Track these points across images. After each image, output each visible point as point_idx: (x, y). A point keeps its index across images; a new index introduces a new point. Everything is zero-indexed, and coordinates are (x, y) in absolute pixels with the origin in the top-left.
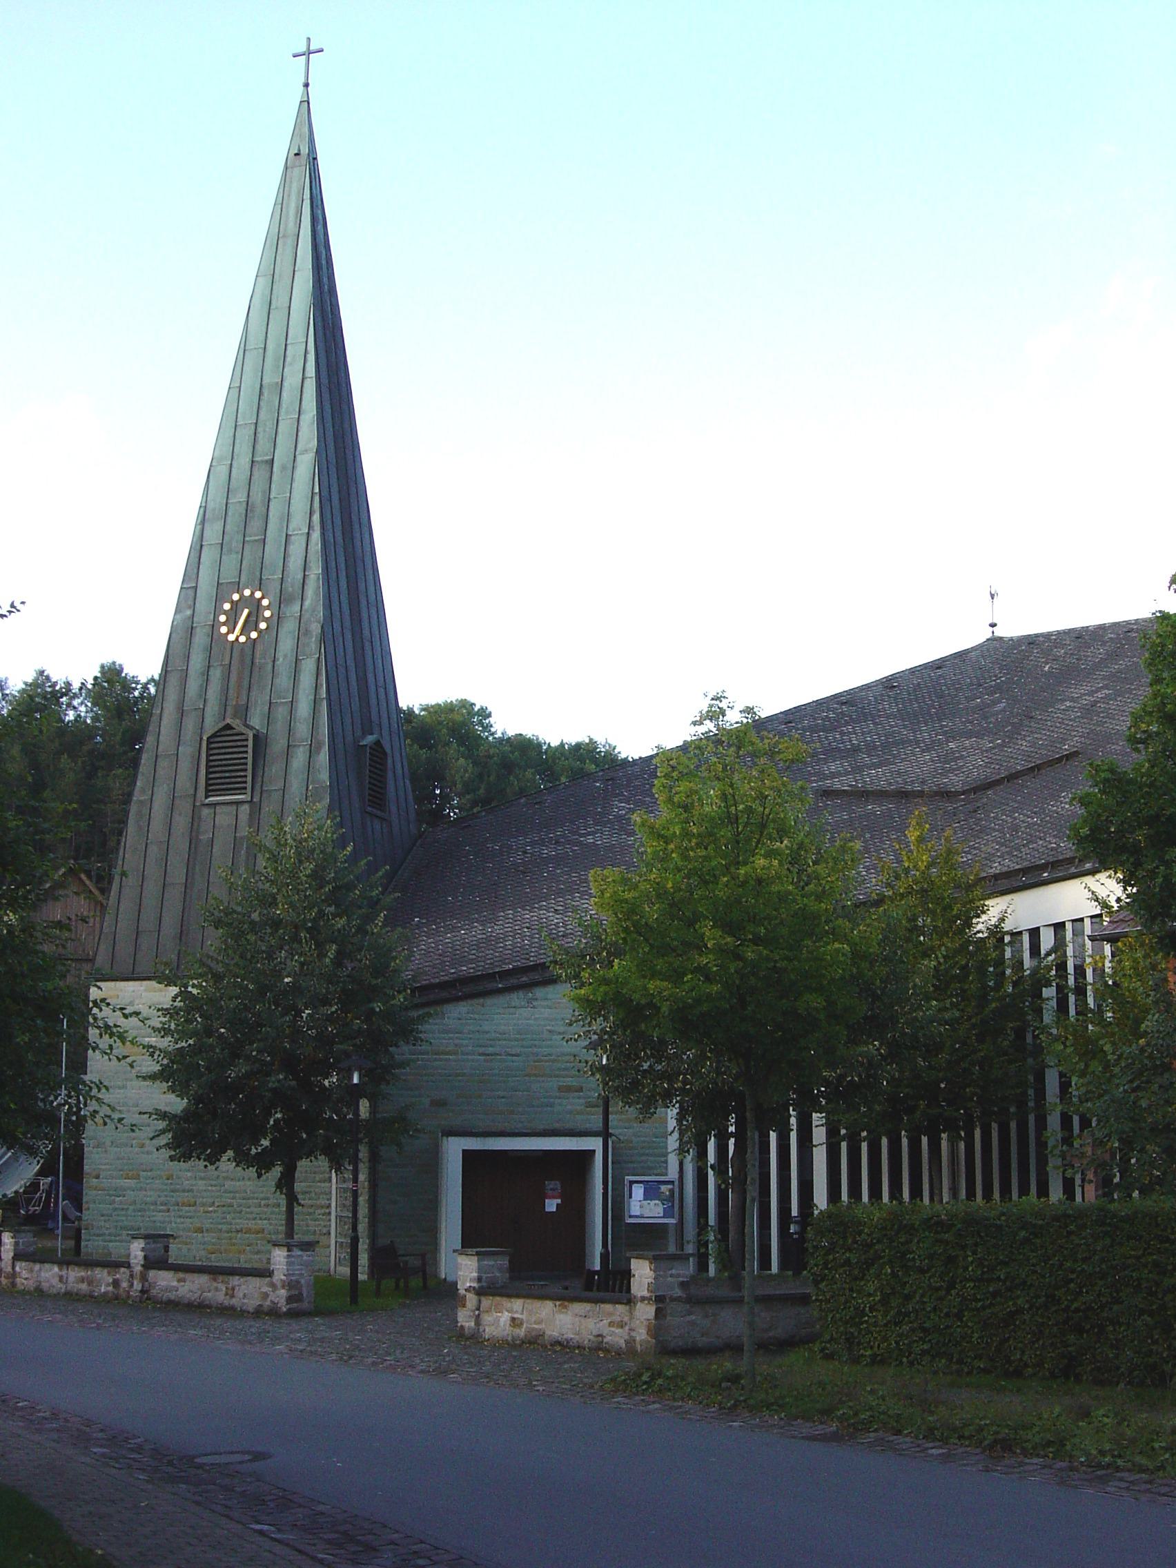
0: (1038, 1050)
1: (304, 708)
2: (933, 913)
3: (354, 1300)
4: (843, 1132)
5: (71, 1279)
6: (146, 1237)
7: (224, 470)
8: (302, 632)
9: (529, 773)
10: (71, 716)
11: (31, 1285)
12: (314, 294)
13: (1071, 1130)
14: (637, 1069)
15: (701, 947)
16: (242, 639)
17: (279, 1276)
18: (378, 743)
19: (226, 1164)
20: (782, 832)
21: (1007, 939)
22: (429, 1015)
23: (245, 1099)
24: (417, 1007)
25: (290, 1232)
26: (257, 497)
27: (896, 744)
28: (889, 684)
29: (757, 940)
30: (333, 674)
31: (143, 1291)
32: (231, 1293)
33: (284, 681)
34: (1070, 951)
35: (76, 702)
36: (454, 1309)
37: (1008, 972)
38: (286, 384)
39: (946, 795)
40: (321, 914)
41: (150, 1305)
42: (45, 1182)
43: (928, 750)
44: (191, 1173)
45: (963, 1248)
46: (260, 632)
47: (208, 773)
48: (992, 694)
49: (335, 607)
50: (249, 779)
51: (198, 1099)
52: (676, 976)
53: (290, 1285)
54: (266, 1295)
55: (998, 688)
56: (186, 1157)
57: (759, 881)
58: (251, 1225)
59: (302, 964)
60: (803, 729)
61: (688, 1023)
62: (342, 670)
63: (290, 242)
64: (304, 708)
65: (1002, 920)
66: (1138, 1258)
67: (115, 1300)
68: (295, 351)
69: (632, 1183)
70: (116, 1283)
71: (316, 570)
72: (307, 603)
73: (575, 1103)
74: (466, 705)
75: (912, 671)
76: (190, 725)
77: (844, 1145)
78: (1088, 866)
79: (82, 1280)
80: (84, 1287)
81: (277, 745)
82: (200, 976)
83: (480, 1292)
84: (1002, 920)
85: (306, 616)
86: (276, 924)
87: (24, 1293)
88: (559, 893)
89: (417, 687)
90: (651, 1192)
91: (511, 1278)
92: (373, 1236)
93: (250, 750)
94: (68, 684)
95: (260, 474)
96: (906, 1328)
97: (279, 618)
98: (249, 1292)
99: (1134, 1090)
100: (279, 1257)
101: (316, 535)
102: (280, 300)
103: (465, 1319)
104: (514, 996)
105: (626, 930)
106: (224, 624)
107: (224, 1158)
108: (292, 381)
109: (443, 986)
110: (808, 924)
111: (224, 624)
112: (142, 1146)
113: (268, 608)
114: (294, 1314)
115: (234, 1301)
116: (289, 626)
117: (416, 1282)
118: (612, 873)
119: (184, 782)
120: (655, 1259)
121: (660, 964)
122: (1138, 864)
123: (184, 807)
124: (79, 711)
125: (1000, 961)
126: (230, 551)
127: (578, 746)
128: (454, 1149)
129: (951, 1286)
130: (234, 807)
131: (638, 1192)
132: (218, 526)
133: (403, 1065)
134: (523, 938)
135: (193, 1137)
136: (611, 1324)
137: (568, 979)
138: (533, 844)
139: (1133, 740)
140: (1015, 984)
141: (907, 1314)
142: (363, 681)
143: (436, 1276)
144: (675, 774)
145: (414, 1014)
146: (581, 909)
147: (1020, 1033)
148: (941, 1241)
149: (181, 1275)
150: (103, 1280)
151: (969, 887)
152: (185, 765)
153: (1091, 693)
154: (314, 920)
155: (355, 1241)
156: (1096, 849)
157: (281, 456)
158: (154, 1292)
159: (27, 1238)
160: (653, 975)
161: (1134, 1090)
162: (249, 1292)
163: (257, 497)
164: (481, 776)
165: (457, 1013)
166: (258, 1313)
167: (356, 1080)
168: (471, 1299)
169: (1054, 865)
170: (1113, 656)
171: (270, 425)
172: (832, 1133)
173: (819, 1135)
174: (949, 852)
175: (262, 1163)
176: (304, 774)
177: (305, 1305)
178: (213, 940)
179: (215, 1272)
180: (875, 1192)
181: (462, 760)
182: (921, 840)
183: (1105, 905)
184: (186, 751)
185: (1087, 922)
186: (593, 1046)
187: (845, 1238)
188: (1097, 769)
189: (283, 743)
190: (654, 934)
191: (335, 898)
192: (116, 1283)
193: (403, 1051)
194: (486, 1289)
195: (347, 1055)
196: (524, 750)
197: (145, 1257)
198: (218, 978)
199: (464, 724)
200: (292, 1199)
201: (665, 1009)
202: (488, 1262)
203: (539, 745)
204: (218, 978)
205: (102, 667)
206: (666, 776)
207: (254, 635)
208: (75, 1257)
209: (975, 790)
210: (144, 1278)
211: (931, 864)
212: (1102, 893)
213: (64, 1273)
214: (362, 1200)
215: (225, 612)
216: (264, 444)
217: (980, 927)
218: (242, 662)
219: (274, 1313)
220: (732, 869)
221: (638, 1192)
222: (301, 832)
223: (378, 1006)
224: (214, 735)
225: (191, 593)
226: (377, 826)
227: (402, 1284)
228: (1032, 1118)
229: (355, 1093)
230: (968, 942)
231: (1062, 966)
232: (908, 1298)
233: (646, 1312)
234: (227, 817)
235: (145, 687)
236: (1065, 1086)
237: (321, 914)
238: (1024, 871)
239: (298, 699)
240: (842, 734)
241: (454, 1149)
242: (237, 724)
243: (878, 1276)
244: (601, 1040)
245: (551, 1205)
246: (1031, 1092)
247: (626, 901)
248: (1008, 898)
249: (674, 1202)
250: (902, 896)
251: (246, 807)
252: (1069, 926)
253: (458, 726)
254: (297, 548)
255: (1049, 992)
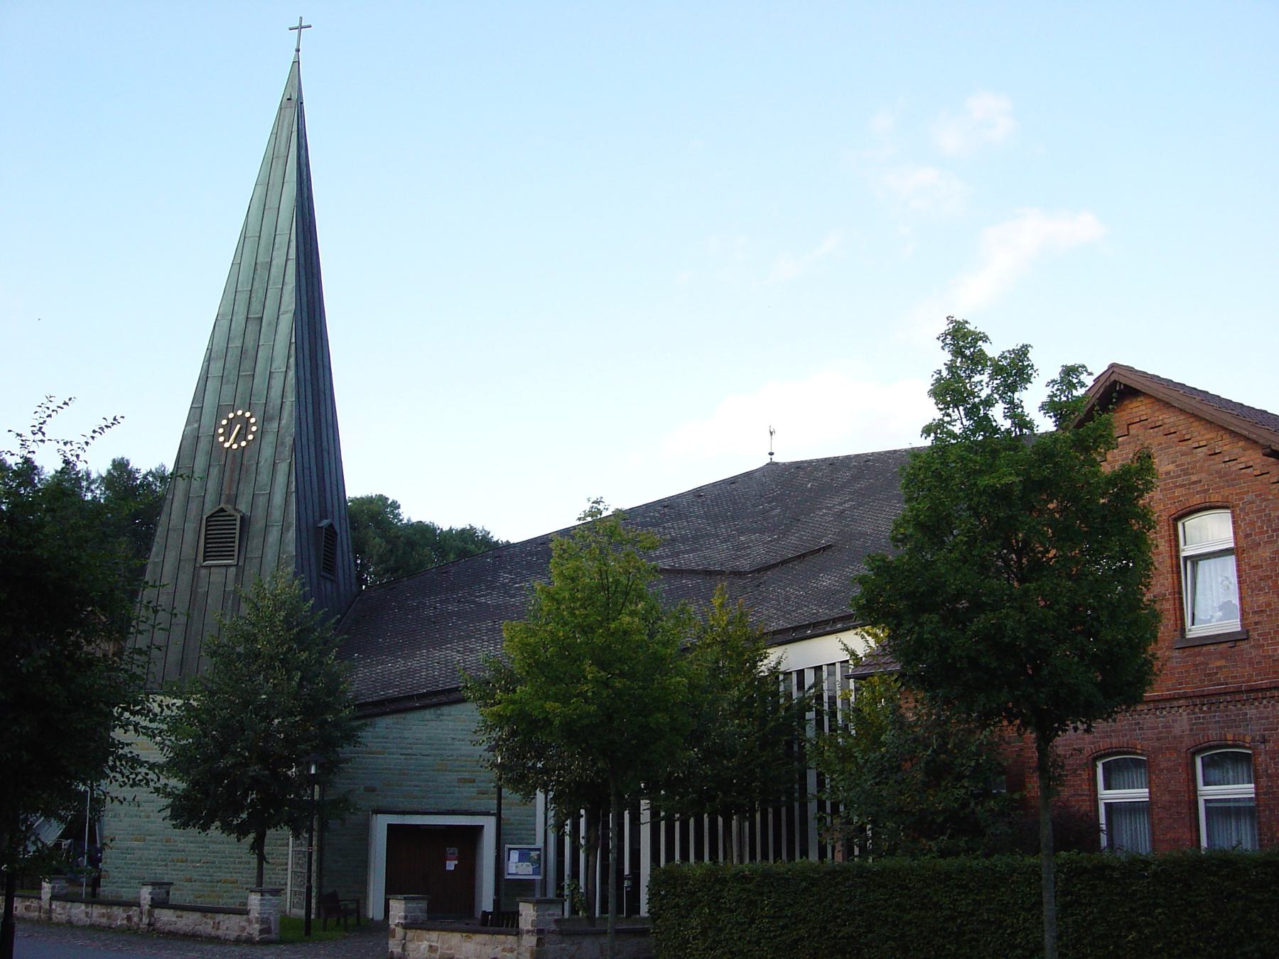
0: (802, 757)
1: (278, 499)
2: (730, 657)
3: (308, 932)
4: (662, 814)
5: (95, 915)
6: (153, 884)
7: (225, 323)
8: (278, 445)
9: (427, 550)
10: (89, 496)
11: (64, 918)
12: (297, 201)
13: (824, 811)
14: (524, 765)
15: (580, 678)
16: (235, 446)
17: (254, 914)
18: (331, 526)
19: (215, 832)
20: (641, 597)
21: (781, 677)
22: (366, 725)
23: (235, 784)
24: (358, 718)
25: (260, 883)
26: (250, 344)
27: (702, 536)
28: (698, 493)
29: (622, 674)
30: (300, 474)
31: (149, 924)
32: (217, 926)
33: (264, 477)
34: (825, 686)
35: (93, 487)
36: (387, 938)
37: (782, 701)
38: (274, 263)
39: (738, 574)
40: (290, 649)
41: (154, 934)
42: (66, 843)
43: (725, 541)
44: (189, 839)
45: (761, 894)
46: (248, 442)
47: (206, 543)
48: (770, 503)
49: (304, 427)
50: (236, 549)
51: (194, 784)
52: (565, 700)
53: (262, 921)
54: (244, 928)
55: (775, 499)
56: (185, 825)
57: (625, 633)
58: (228, 877)
59: (275, 685)
60: (637, 524)
61: (572, 732)
62: (307, 471)
63: (281, 161)
64: (278, 499)
65: (779, 663)
66: (886, 900)
67: (129, 932)
68: (282, 240)
69: (510, 849)
70: (129, 918)
71: (291, 398)
72: (283, 422)
73: (469, 790)
74: (382, 499)
75: (714, 485)
76: (194, 506)
77: (663, 823)
78: (839, 626)
79: (103, 915)
80: (104, 920)
81: (258, 525)
82: (201, 692)
83: (406, 927)
84: (779, 663)
85: (282, 431)
86: (258, 655)
87: (58, 924)
88: (460, 638)
89: (357, 485)
90: (524, 857)
91: (429, 919)
92: (320, 887)
93: (238, 527)
94: (88, 474)
95: (252, 327)
96: (719, 952)
97: (262, 433)
98: (230, 926)
99: (877, 784)
100: (254, 900)
101: (292, 373)
102: (272, 202)
103: (394, 946)
104: (427, 712)
105: (529, 665)
106: (221, 435)
107: (213, 827)
108: (279, 261)
109: (375, 704)
110: (658, 662)
111: (221, 435)
112: (148, 817)
113: (254, 424)
114: (264, 942)
115: (220, 933)
116: (270, 438)
117: (352, 920)
118: (519, 625)
119: (188, 550)
120: (537, 903)
121: (553, 690)
122: (899, 625)
123: (188, 567)
124: (96, 493)
125: (776, 694)
126: (228, 382)
127: (463, 530)
128: (381, 824)
129: (753, 920)
130: (223, 570)
131: (514, 856)
132: (220, 364)
133: (347, 761)
134: (434, 669)
135: (188, 812)
136: (503, 950)
137: (475, 700)
138: (441, 602)
139: (895, 539)
140: (787, 709)
141: (720, 942)
142: (321, 480)
143: (365, 916)
144: (566, 555)
145: (355, 723)
146: (490, 649)
147: (789, 744)
148: (745, 890)
149: (179, 913)
150: (120, 915)
151: (756, 640)
152: (189, 537)
153: (841, 504)
154: (284, 654)
155: (309, 889)
156: (867, 613)
157: (268, 315)
158: (158, 925)
159: (61, 884)
160: (547, 698)
161: (877, 784)
162: (230, 926)
163: (250, 344)
164: (391, 551)
165: (385, 725)
166: (238, 941)
167: (313, 771)
168: (399, 932)
169: (815, 625)
170: (855, 478)
171: (261, 292)
172: (655, 814)
173: (645, 816)
174: (742, 614)
175: (242, 831)
176: (277, 546)
177: (273, 936)
178: (207, 666)
179: (204, 911)
180: (699, 856)
181: (377, 540)
182: (722, 605)
183: (853, 654)
184: (191, 526)
185: (838, 665)
186: (491, 749)
187: (675, 888)
188: (873, 560)
189: (261, 523)
190: (551, 668)
191: (299, 639)
192: (129, 918)
193: (346, 751)
194: (411, 924)
195: (307, 753)
196: (423, 532)
197: (152, 899)
198: (212, 693)
199: (379, 513)
200: (262, 859)
201: (557, 722)
202: (412, 905)
203: (435, 530)
204: (212, 693)
205: (114, 461)
206: (560, 556)
207: (243, 444)
208: (93, 898)
209: (759, 571)
210: (150, 914)
211: (730, 623)
212: (851, 646)
213: (89, 910)
214: (314, 857)
215: (223, 426)
216: (256, 306)
217: (763, 668)
218: (234, 462)
219: (249, 941)
220: (605, 624)
221: (514, 856)
222: (276, 589)
223: (330, 718)
224: (211, 516)
225: (198, 411)
226: (328, 585)
227: (342, 920)
228: (797, 805)
229: (313, 780)
230: (755, 679)
231: (819, 697)
232: (721, 930)
233: (530, 941)
234: (219, 575)
235: (145, 477)
236: (821, 784)
237: (290, 649)
238: (795, 629)
239: (274, 492)
240: (664, 528)
241: (381, 824)
242: (229, 508)
243: (699, 915)
244: (497, 746)
245: (451, 865)
246: (797, 786)
247: (529, 644)
248: (783, 648)
249: (540, 864)
250: (709, 645)
251: (233, 569)
252: (825, 668)
253: (377, 512)
254: (277, 383)
255: (810, 715)
